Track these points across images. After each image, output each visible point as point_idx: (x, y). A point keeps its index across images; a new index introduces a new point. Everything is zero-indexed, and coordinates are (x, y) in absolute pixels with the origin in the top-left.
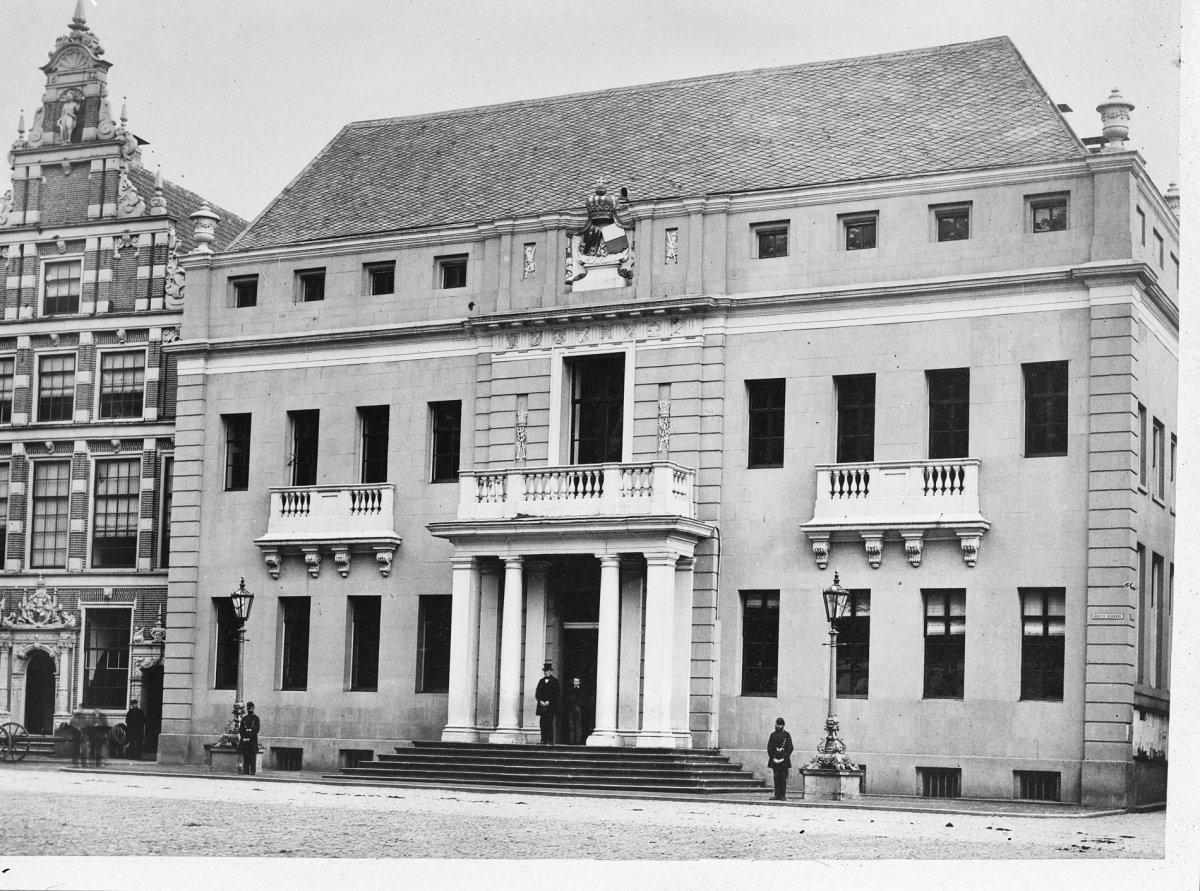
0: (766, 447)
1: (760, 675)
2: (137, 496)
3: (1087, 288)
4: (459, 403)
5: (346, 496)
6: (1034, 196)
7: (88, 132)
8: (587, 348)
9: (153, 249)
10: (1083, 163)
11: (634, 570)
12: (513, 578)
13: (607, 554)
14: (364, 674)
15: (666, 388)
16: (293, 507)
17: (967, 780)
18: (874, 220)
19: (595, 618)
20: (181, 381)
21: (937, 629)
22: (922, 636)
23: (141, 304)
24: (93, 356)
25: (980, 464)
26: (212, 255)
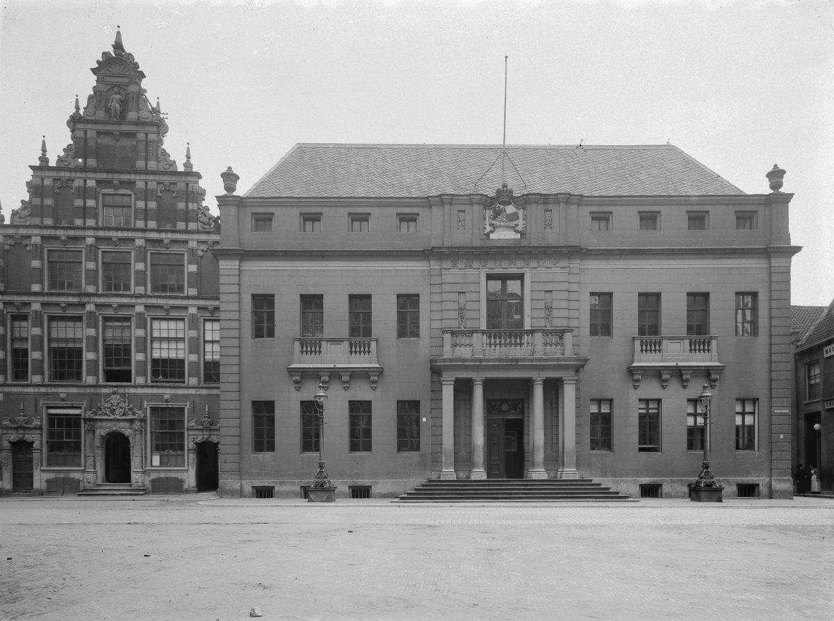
2: (26, 339)
5: (346, 344)
6: (402, 214)
7: (132, 115)
8: (516, 269)
9: (146, 191)
11: (553, 389)
13: (539, 377)
18: (656, 217)
20: (221, 272)
23: (79, 222)
24: (42, 253)
25: (377, 340)
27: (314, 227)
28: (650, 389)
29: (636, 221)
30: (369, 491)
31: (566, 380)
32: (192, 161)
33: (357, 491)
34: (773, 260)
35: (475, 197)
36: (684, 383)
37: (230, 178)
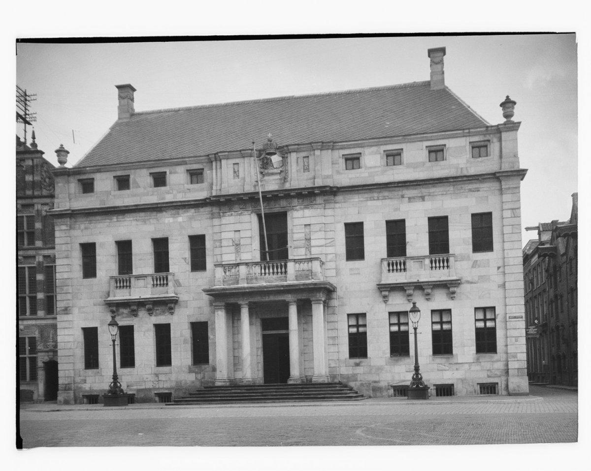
0: (89, 270)
4: (490, 214)
5: (150, 280)
6: (387, 151)
12: (245, 313)
15: (308, 227)
22: (431, 330)
27: (395, 160)
28: (399, 303)
29: (425, 153)
31: (313, 301)
32: (36, 142)
34: (503, 183)
36: (428, 297)
37: (62, 152)
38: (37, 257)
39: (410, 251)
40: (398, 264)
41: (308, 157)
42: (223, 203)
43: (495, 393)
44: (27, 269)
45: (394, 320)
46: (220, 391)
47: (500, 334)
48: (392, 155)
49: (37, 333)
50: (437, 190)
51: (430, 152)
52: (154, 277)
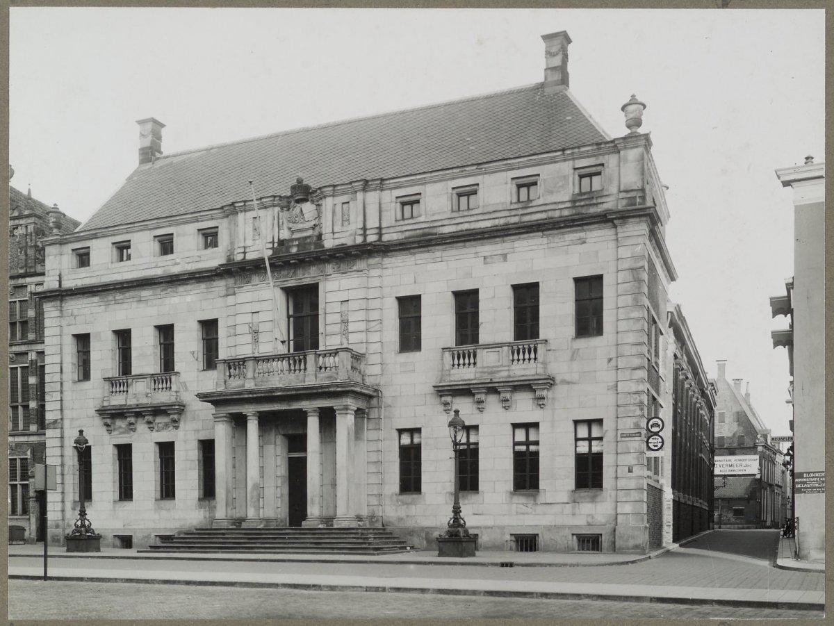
0: (410, 338)
1: (411, 481)
3: (615, 227)
10: (613, 145)
11: (328, 420)
12: (253, 426)
14: (167, 490)
15: (345, 304)
16: (118, 389)
17: (541, 541)
19: (305, 450)
21: (583, 448)
22: (574, 454)
26: (61, 236)
27: (530, 192)
30: (598, 540)
33: (526, 541)
35: (356, 184)
38: (30, 354)
39: (484, 336)
40: (532, 350)
41: (348, 202)
42: (239, 270)
43: (598, 550)
44: (19, 370)
45: (583, 432)
46: (352, 536)
47: (608, 461)
48: (525, 186)
49: (29, 453)
50: (146, 293)
51: (519, 186)
52: (455, 352)
